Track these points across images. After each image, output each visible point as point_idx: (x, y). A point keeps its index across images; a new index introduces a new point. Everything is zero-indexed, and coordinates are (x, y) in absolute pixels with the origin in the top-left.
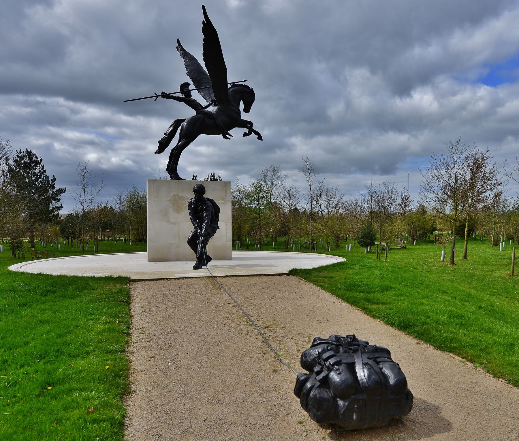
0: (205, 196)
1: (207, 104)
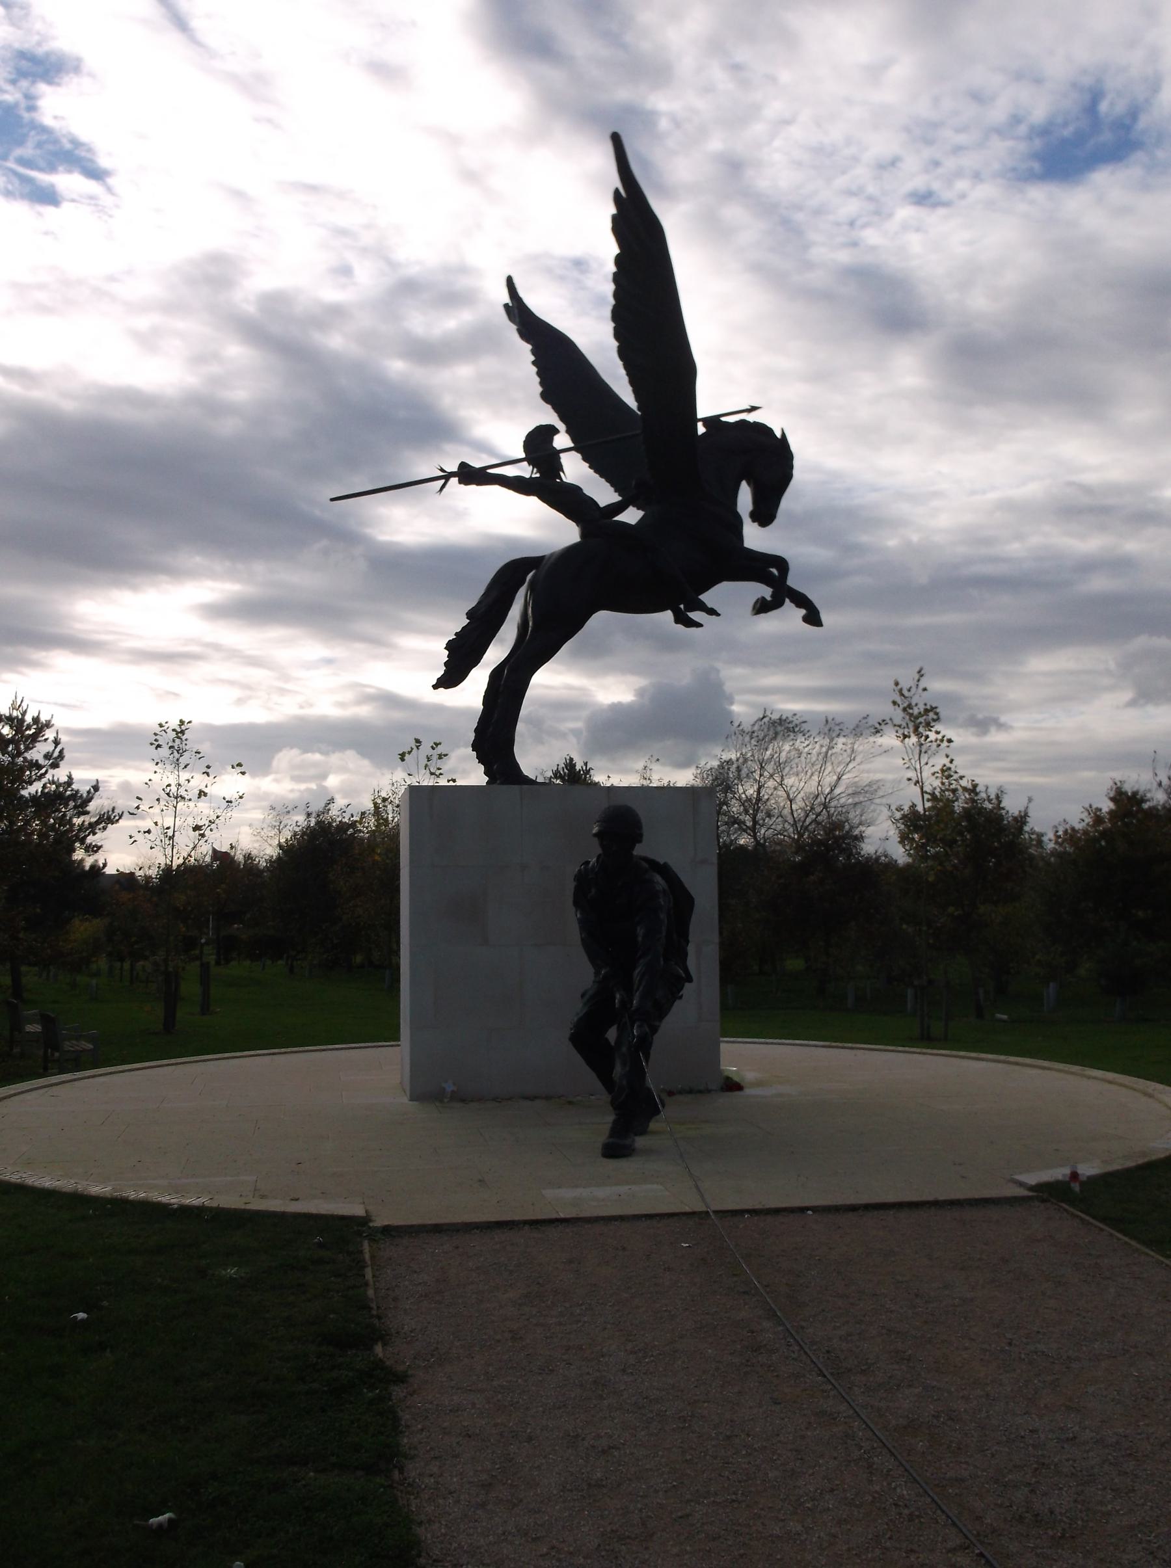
0: (639, 850)
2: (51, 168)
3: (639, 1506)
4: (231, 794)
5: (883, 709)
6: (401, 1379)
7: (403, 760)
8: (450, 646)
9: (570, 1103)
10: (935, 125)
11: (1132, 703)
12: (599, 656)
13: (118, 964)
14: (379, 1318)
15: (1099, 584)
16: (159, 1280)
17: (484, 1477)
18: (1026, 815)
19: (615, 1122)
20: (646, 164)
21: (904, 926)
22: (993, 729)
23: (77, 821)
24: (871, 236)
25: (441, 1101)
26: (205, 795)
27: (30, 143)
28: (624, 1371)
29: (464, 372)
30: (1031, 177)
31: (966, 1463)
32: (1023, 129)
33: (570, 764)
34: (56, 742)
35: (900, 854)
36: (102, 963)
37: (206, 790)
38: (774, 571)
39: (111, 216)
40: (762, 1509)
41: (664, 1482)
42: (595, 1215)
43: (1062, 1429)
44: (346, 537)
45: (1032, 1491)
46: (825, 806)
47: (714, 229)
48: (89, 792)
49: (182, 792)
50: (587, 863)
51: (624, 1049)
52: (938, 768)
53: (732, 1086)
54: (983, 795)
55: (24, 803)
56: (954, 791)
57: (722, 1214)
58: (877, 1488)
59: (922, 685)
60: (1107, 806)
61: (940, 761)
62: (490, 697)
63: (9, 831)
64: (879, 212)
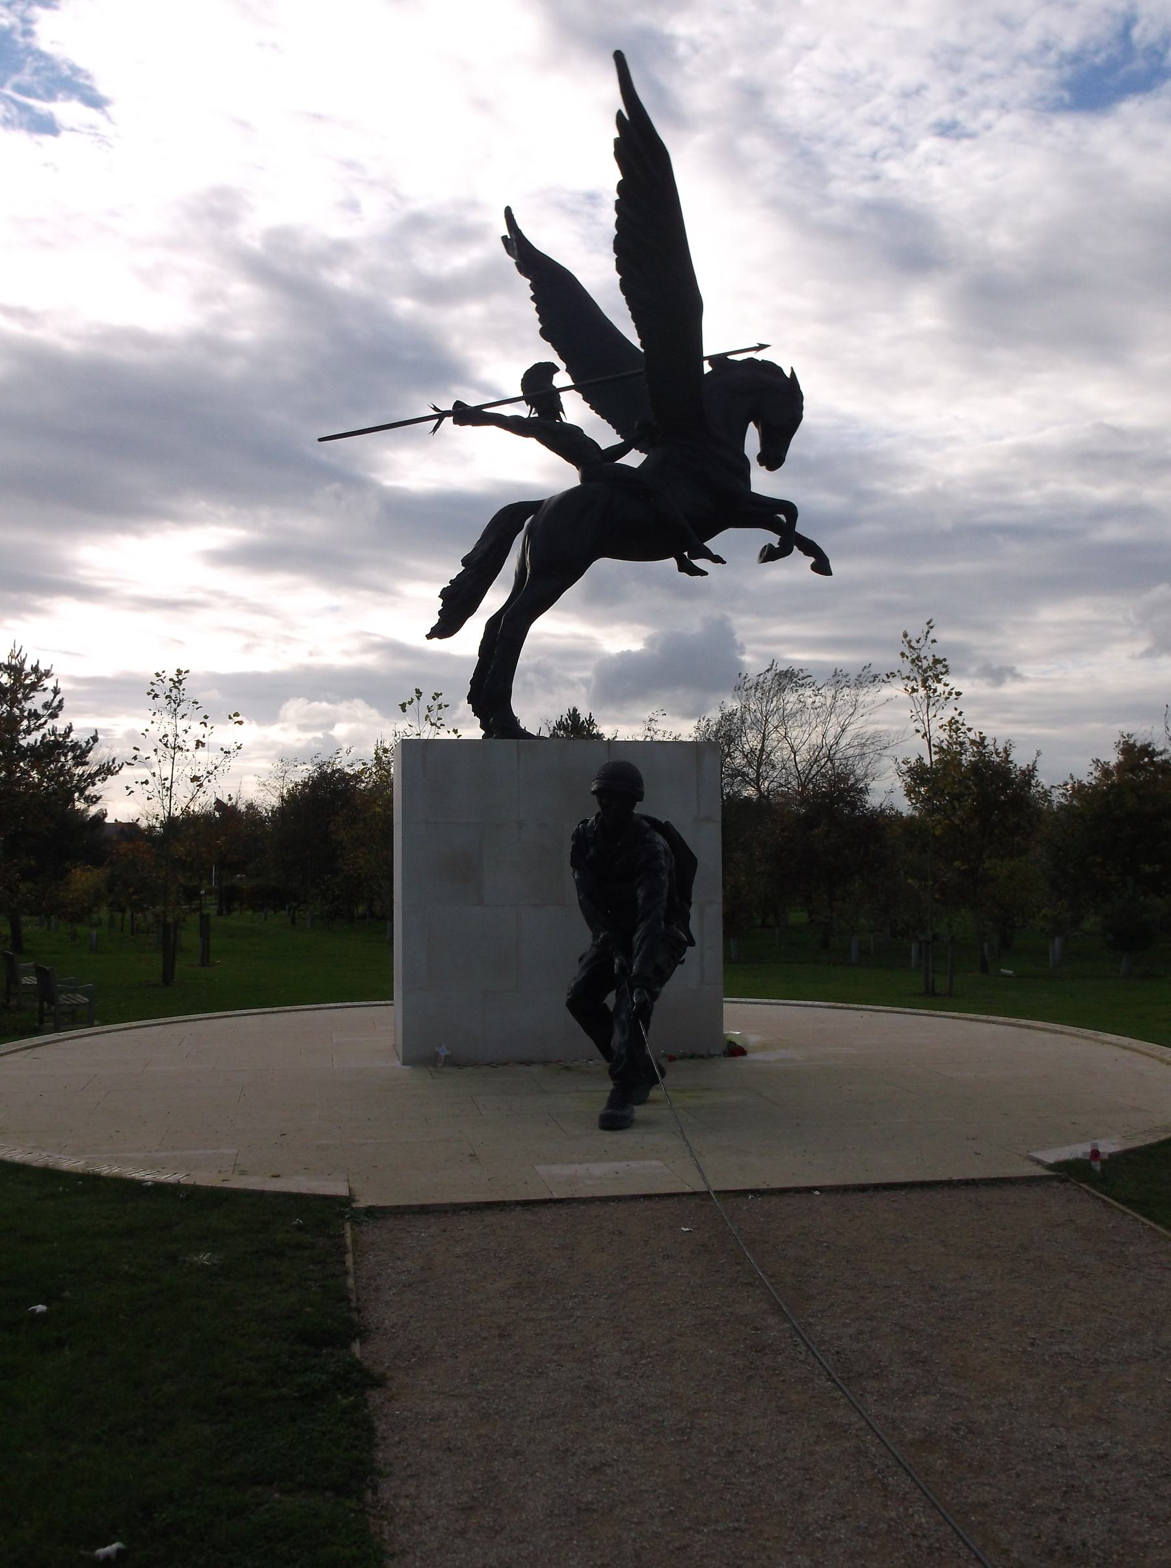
0: (639, 809)
1: (618, 440)
2: (50, 96)
3: (633, 1534)
4: (229, 744)
5: (889, 659)
6: (379, 1382)
7: (404, 711)
8: (444, 594)
9: (567, 1068)
10: (961, 51)
11: (1148, 654)
12: (607, 601)
13: (119, 915)
14: (358, 1310)
15: (1113, 532)
16: (126, 1267)
17: (465, 1498)
18: (1034, 768)
19: (613, 1092)
20: (660, 92)
21: (910, 881)
22: (1009, 679)
23: (79, 771)
24: (893, 169)
25: (435, 1066)
26: (203, 745)
27: (27, 71)
28: (618, 1374)
29: (474, 311)
30: (1059, 107)
31: (990, 1485)
32: (1052, 57)
33: (574, 715)
34: (56, 691)
35: (904, 806)
36: (104, 913)
37: (203, 740)
38: (782, 517)
39: (111, 146)
40: (767, 1539)
41: (661, 1506)
42: (590, 1195)
43: (1091, 1444)
44: (352, 481)
45: (1062, 1519)
46: (830, 759)
47: (730, 161)
48: (88, 743)
49: (179, 742)
50: (586, 821)
51: (623, 1017)
52: (945, 721)
53: (735, 1050)
54: (991, 748)
55: (24, 753)
56: (962, 744)
57: (724, 1194)
58: (893, 1514)
59: (931, 637)
60: (1113, 758)
61: (948, 713)
62: (487, 647)
63: (9, 780)
64: (903, 143)
